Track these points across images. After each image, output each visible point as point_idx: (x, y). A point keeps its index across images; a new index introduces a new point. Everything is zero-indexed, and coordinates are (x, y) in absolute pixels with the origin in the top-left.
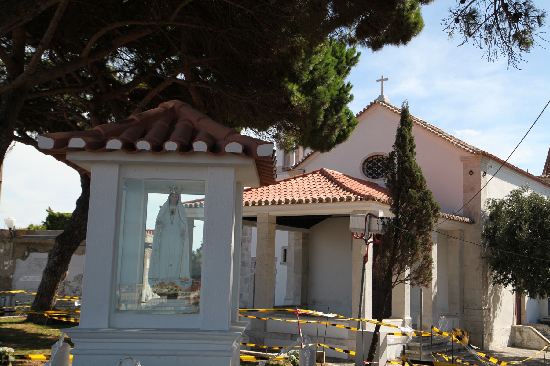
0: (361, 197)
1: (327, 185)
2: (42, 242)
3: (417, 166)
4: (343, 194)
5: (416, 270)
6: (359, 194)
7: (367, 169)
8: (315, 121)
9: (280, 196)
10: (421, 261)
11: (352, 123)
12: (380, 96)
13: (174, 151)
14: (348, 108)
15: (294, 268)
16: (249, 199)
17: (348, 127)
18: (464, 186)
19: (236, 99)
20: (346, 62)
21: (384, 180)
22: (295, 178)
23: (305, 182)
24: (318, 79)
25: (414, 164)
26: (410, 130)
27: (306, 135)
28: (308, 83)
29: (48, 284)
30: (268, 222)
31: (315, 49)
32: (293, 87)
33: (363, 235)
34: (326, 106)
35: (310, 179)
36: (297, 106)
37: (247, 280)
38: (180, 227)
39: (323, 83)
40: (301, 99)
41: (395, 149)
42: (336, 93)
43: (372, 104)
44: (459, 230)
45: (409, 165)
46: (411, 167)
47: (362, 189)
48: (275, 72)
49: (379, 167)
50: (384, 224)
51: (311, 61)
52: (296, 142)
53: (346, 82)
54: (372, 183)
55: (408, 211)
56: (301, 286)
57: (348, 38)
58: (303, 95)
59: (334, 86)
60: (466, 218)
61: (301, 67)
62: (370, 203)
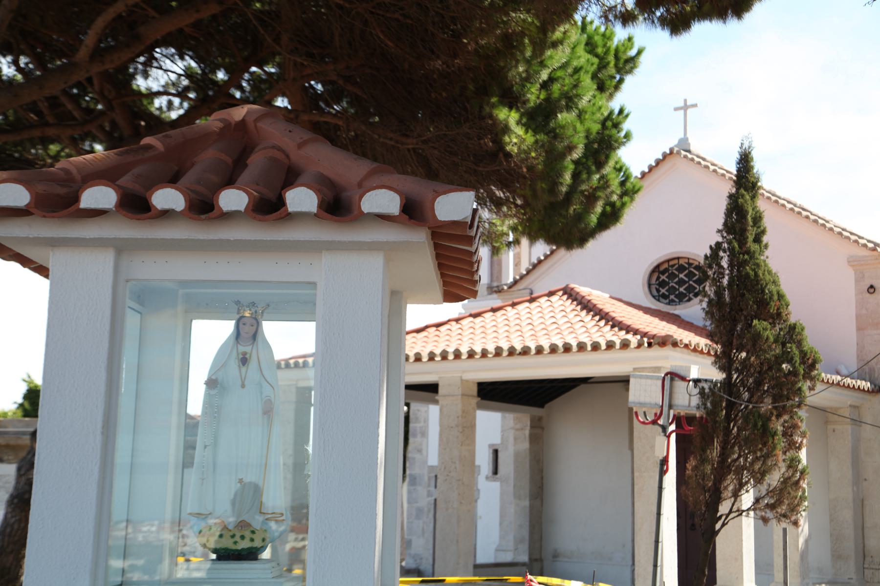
0: (649, 339)
1: (579, 318)
2: (12, 443)
3: (770, 272)
4: (613, 335)
5: (771, 489)
6: (645, 335)
7: (657, 287)
8: (554, 185)
9: (484, 340)
10: (783, 470)
11: (629, 191)
12: (681, 141)
13: (239, 212)
14: (620, 158)
15: (515, 486)
16: (423, 349)
17: (621, 197)
18: (858, 317)
19: (393, 143)
20: (616, 66)
21: (701, 301)
22: (514, 305)
23: (534, 312)
24: (559, 100)
25: (763, 268)
26: (754, 197)
27: (535, 216)
28: (538, 108)
29: (16, 526)
30: (460, 393)
31: (551, 37)
32: (508, 116)
33: (658, 417)
34: (576, 154)
35: (544, 306)
36: (516, 154)
37: (420, 511)
38: (261, 393)
39: (568, 108)
40: (524, 140)
41: (723, 237)
42: (596, 128)
43: (665, 156)
44: (850, 406)
45: (754, 270)
46: (756, 275)
47: (650, 325)
48: (471, 87)
49: (681, 282)
50: (702, 393)
51: (545, 62)
52: (514, 229)
53: (615, 105)
54: (668, 313)
55: (751, 366)
56: (528, 524)
57: (621, 11)
58: (530, 131)
59: (593, 114)
60: (864, 382)
61: (524, 75)
62: (668, 351)
